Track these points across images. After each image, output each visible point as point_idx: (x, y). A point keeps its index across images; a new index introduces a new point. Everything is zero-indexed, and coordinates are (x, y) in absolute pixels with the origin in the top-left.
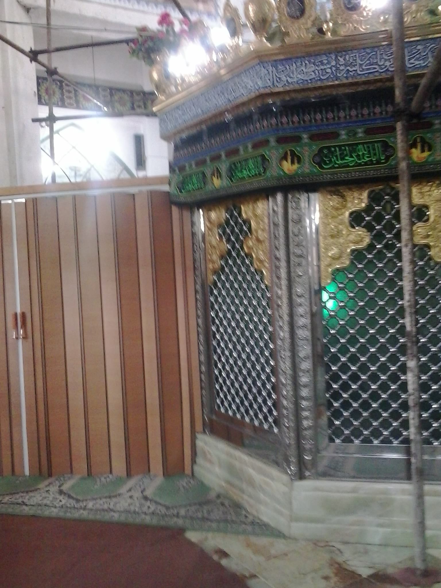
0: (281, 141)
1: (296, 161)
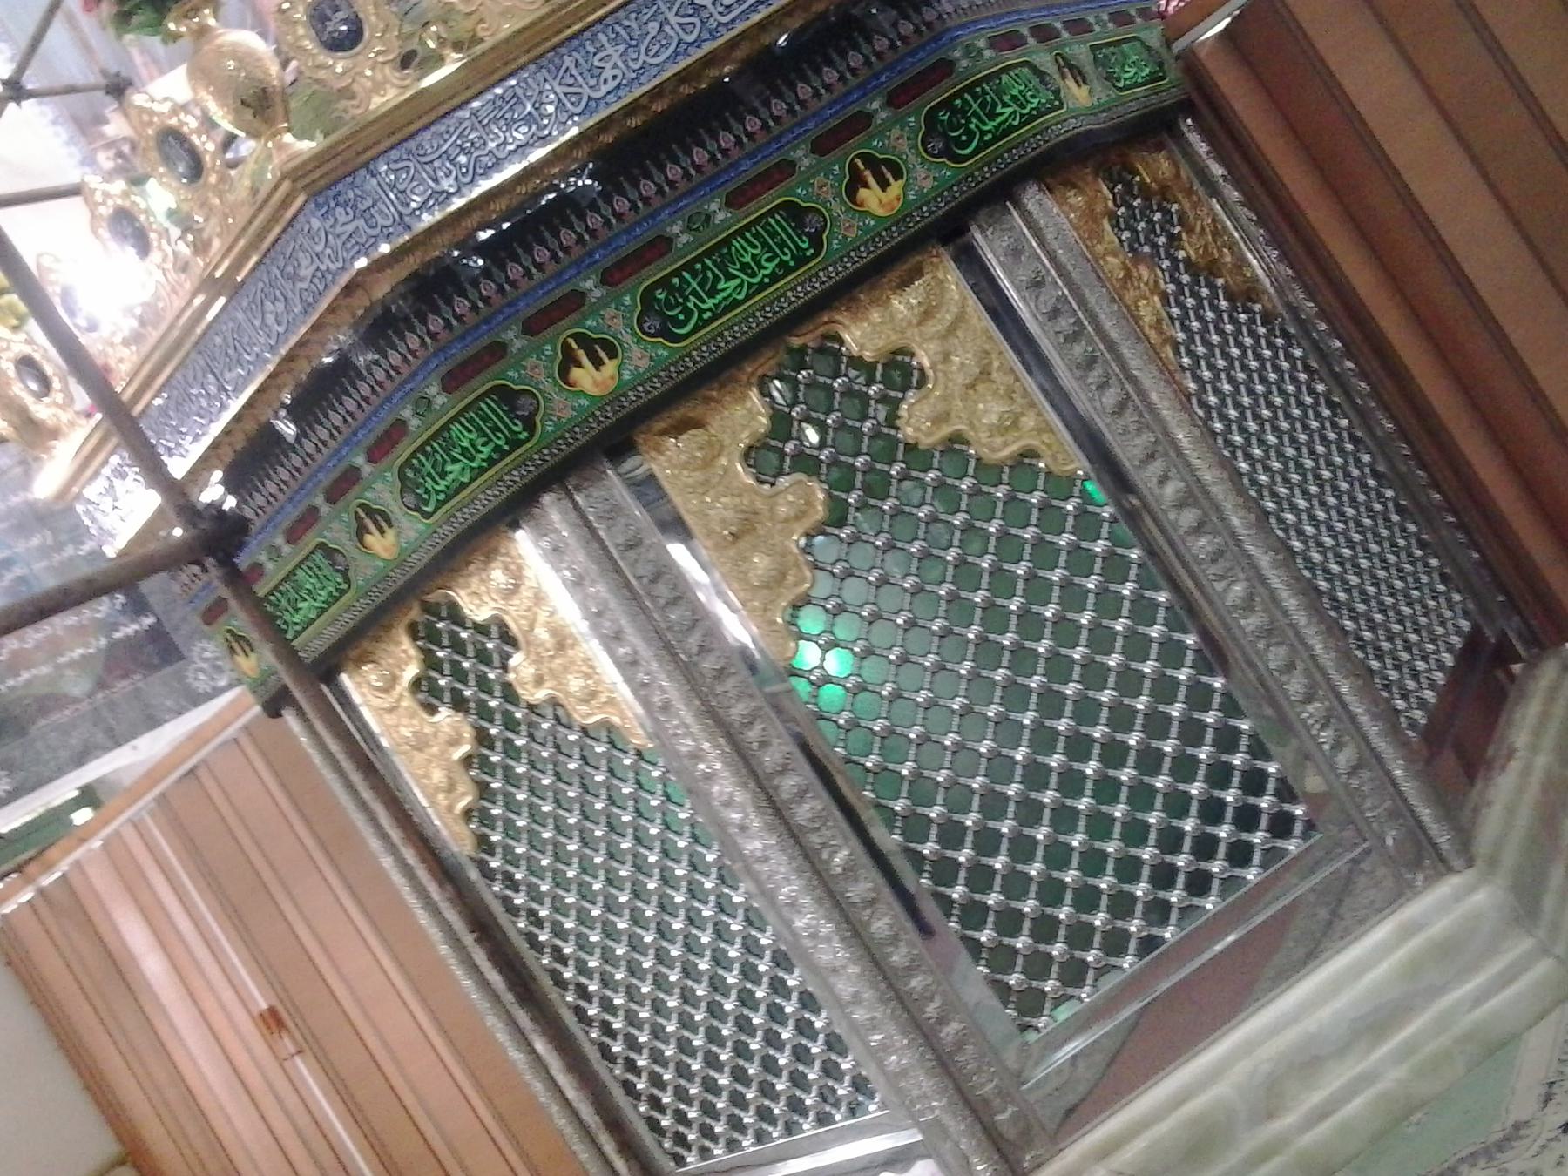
1: (603, 355)
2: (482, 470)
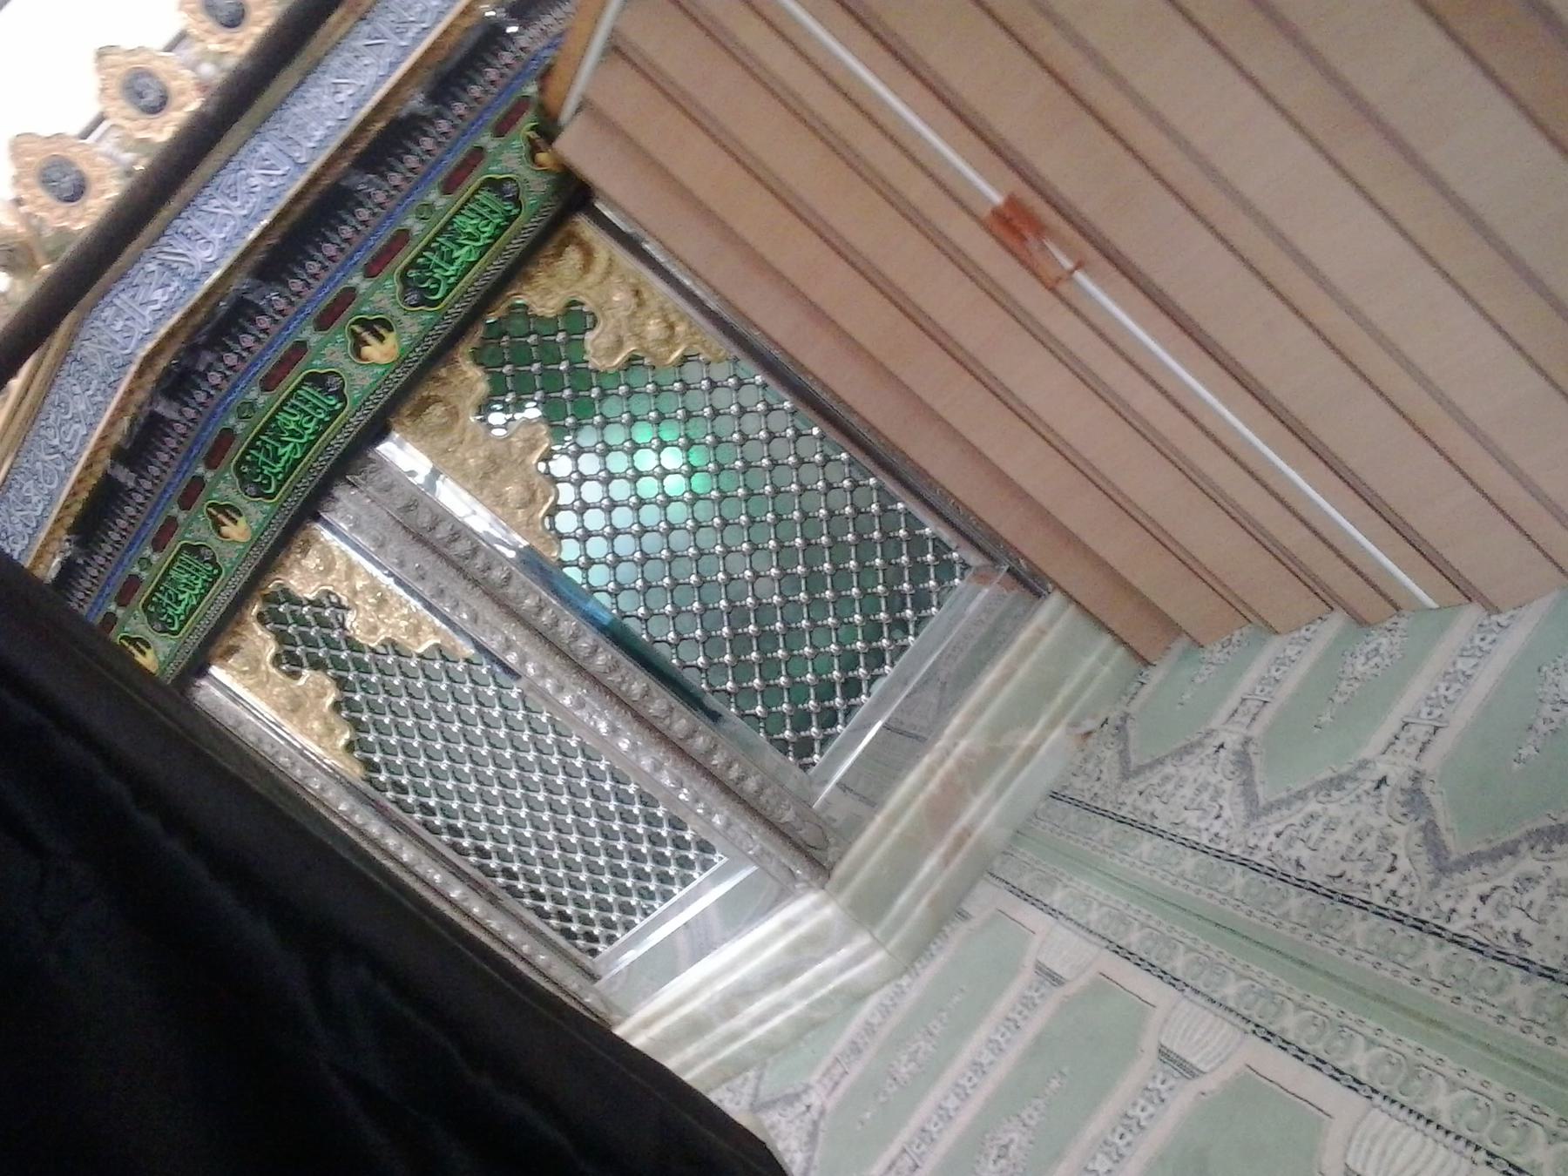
0: (325, 321)
1: (382, 331)
2: (488, 246)
